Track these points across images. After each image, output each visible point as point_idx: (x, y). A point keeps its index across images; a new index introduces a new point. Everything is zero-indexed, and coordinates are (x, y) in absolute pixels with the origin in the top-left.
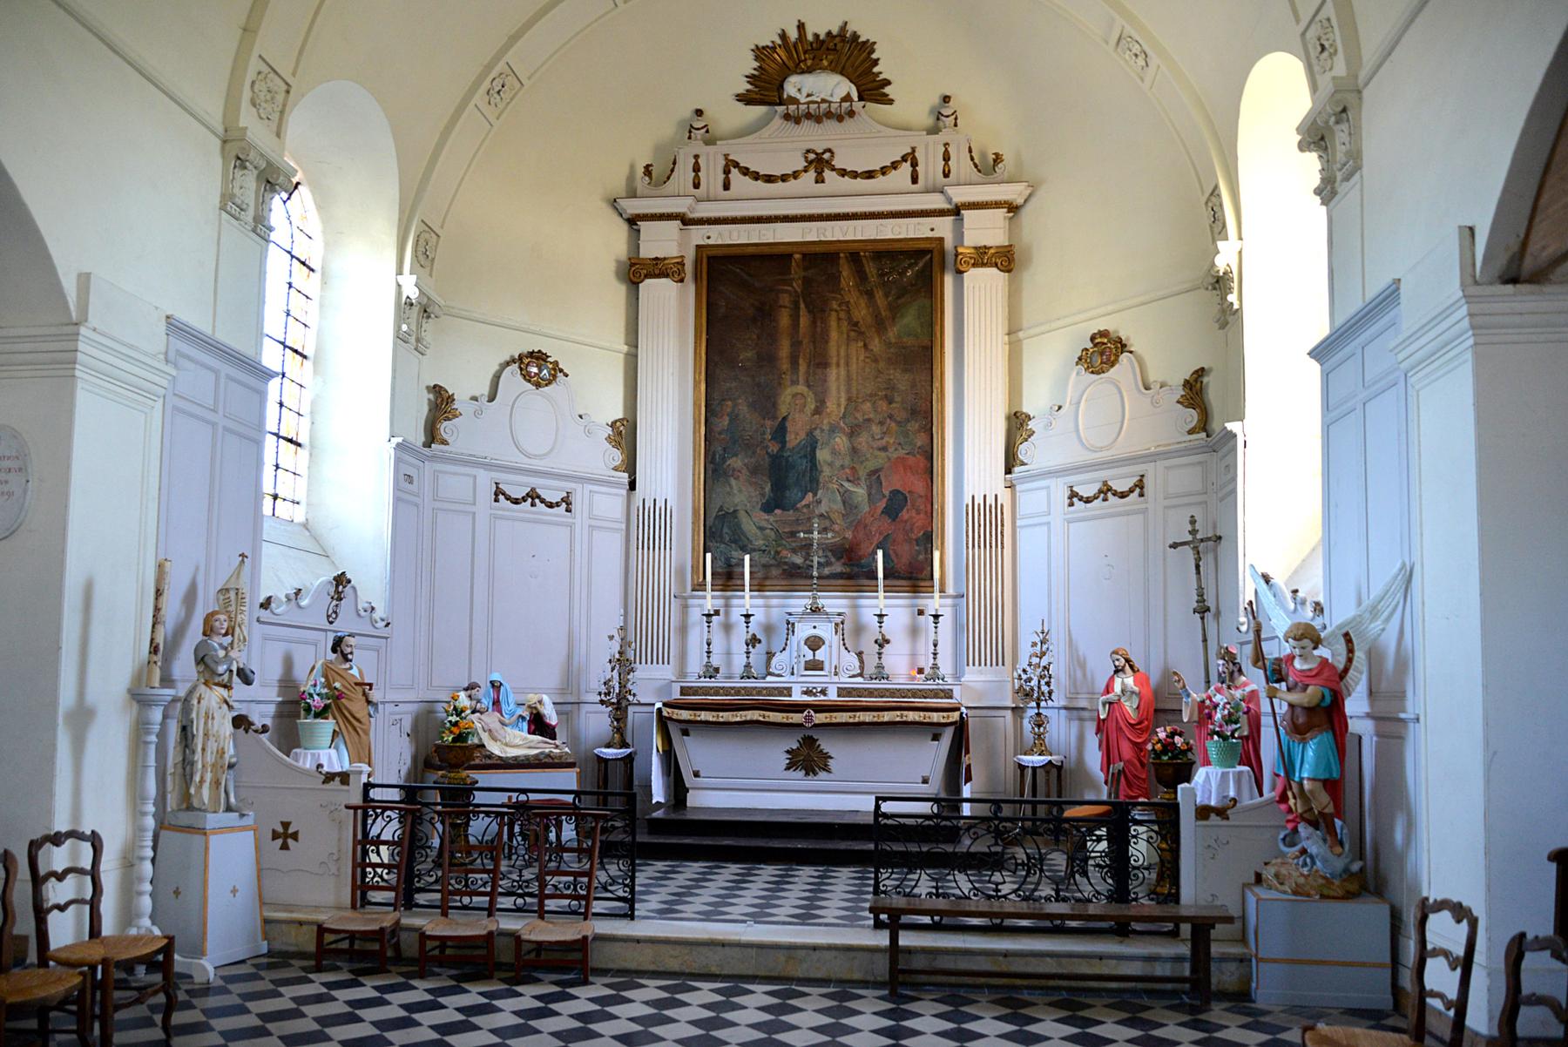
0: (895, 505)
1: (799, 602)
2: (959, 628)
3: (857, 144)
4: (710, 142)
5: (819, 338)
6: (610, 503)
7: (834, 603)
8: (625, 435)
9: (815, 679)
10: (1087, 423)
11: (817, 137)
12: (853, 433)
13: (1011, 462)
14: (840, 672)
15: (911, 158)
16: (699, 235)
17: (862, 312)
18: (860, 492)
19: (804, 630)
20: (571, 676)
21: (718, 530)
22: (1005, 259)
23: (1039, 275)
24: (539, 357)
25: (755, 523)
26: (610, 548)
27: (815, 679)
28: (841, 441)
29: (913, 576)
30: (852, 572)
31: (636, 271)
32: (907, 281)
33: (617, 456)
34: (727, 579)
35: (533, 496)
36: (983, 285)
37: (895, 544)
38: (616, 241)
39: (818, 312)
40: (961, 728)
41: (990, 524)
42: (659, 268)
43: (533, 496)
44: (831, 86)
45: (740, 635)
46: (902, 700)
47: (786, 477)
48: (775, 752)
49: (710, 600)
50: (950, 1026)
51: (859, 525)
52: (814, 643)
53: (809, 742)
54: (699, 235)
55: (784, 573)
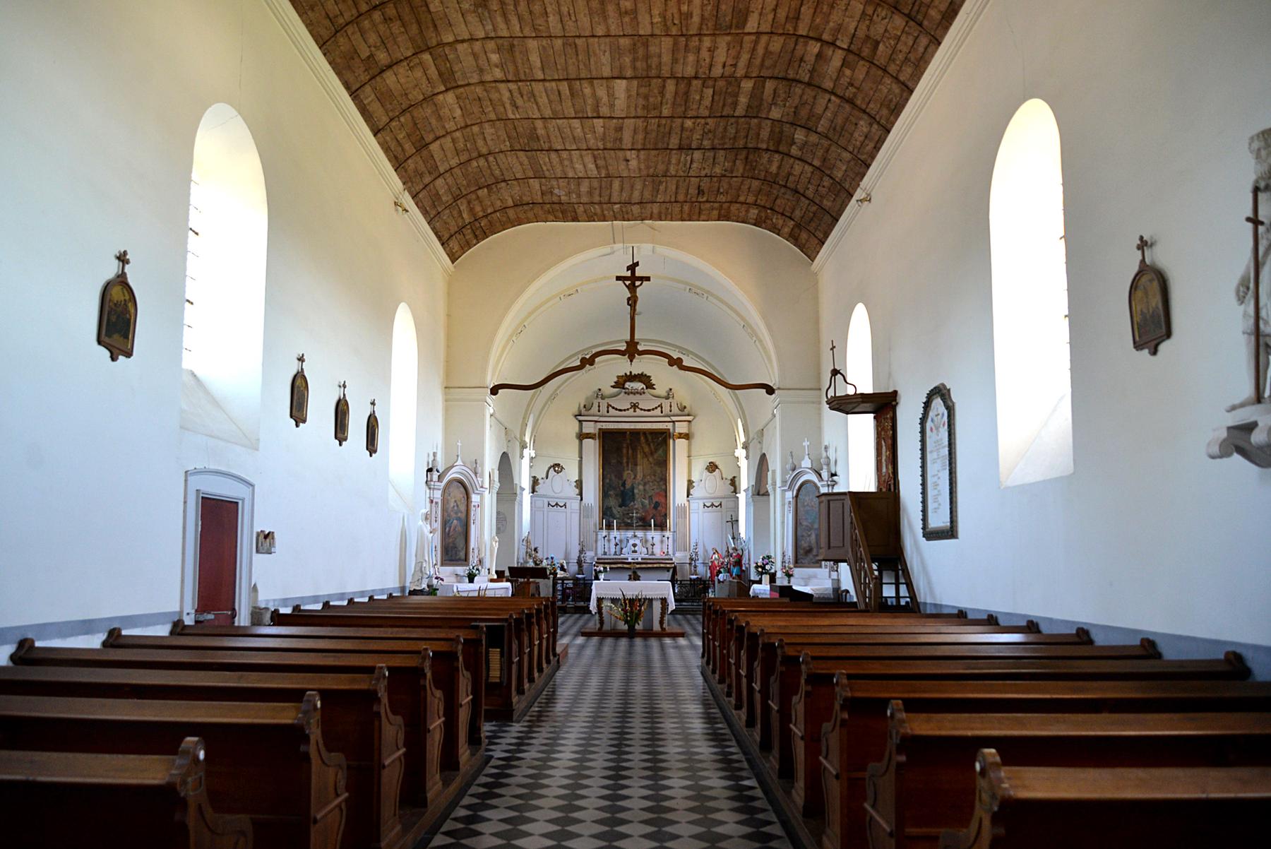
0: (657, 505)
1: (630, 534)
2: (674, 541)
3: (646, 402)
4: (603, 398)
5: (635, 457)
6: (575, 505)
7: (640, 534)
8: (579, 484)
9: (635, 555)
10: (707, 486)
11: (634, 399)
12: (645, 484)
14: (642, 554)
15: (661, 406)
16: (599, 426)
17: (647, 450)
18: (647, 502)
19: (631, 542)
21: (606, 513)
22: (687, 436)
23: (696, 441)
24: (558, 465)
25: (616, 510)
26: (576, 517)
28: (641, 487)
29: (662, 526)
30: (645, 526)
31: (582, 436)
32: (660, 440)
33: (577, 491)
34: (609, 527)
36: (681, 444)
39: (634, 450)
40: (675, 568)
41: (683, 511)
42: (588, 436)
44: (639, 386)
45: (613, 542)
46: (659, 561)
47: (625, 497)
49: (604, 533)
50: (702, 830)
51: (647, 511)
52: (634, 545)
53: (635, 573)
54: (599, 426)
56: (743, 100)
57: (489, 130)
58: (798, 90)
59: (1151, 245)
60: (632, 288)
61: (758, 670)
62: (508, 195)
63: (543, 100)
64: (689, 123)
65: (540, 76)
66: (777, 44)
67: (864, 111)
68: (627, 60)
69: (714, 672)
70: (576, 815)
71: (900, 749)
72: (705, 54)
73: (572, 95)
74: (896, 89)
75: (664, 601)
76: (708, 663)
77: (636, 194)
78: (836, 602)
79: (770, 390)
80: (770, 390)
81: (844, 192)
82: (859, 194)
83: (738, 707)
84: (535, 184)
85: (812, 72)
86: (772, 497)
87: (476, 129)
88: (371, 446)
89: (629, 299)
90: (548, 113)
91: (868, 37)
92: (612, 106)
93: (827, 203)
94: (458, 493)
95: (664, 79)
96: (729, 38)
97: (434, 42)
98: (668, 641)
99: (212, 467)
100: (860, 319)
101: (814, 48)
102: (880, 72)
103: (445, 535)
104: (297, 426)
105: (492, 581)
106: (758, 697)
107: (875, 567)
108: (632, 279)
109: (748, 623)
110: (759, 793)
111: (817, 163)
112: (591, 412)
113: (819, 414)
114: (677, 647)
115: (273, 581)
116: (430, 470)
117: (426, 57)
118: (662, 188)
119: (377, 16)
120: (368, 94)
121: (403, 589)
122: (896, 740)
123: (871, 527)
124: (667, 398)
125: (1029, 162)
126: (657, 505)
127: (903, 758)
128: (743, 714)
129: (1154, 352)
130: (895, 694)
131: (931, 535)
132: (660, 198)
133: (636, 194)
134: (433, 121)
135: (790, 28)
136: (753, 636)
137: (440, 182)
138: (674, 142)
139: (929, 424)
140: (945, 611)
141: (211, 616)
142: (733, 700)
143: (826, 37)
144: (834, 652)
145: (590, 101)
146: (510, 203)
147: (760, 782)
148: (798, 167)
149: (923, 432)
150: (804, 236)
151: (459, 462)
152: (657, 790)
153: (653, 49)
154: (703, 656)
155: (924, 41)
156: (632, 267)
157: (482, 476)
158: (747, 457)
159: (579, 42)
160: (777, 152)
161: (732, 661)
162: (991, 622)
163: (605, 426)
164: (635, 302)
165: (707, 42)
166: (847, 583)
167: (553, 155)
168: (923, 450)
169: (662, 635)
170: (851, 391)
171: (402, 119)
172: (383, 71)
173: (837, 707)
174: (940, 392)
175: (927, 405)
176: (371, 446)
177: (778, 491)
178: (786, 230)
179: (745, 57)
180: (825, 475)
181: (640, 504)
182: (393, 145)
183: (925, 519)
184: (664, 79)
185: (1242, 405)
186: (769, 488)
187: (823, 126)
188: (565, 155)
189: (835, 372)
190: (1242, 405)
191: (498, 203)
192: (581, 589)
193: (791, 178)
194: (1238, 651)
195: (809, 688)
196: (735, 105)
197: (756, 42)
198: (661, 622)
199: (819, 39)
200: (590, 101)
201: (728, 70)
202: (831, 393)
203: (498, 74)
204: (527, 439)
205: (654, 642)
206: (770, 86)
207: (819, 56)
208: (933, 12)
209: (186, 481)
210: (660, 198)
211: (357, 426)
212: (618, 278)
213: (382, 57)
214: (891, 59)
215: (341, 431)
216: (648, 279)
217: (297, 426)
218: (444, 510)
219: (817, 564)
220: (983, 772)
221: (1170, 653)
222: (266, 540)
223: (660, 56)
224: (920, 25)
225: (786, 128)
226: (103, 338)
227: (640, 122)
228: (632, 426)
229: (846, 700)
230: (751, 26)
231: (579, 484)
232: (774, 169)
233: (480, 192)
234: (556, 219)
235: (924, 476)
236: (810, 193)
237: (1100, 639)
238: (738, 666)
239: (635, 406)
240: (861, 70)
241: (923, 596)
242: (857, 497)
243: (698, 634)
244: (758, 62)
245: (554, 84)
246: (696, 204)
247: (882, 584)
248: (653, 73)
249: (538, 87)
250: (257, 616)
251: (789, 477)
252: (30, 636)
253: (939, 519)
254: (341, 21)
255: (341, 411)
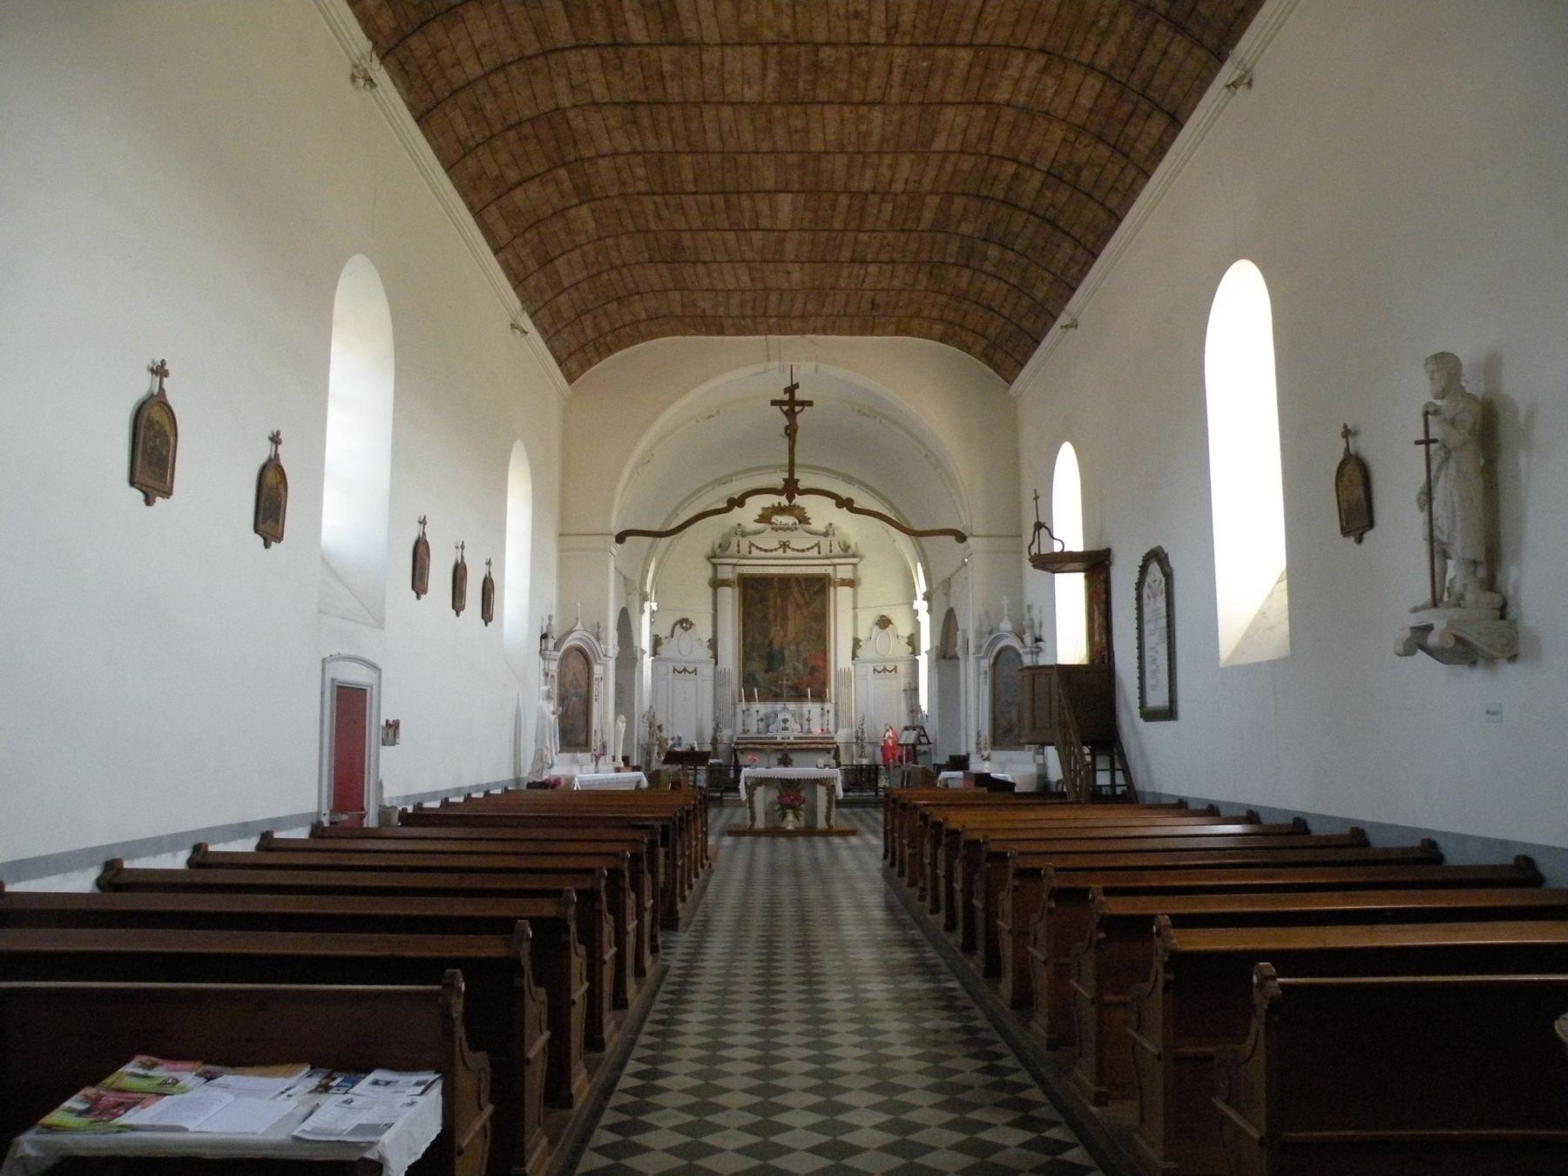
1: (779, 706)
3: (799, 540)
4: (744, 534)
5: (784, 607)
6: (707, 671)
7: (791, 706)
8: (713, 644)
9: (785, 733)
12: (797, 644)
13: (854, 656)
14: (794, 732)
15: (818, 545)
17: (801, 601)
18: (800, 666)
20: (700, 735)
21: (748, 680)
22: (851, 583)
23: (863, 590)
27: (785, 733)
28: (793, 647)
29: (820, 697)
30: (799, 696)
31: (716, 584)
32: (818, 587)
33: (710, 653)
35: (685, 670)
37: (812, 682)
38: (707, 572)
39: (784, 599)
42: (725, 583)
43: (685, 670)
47: (773, 660)
48: (775, 758)
49: (744, 705)
52: (785, 721)
55: (777, 697)
56: (928, 215)
57: (625, 242)
58: (992, 207)
59: (1356, 433)
60: (791, 415)
61: (960, 869)
62: (640, 308)
63: (694, 212)
64: (864, 237)
65: (691, 188)
66: (967, 164)
67: (1068, 234)
68: (795, 175)
69: (901, 874)
70: (724, 1053)
71: (1100, 927)
72: (884, 170)
73: (728, 208)
74: (1103, 215)
75: (831, 790)
76: (892, 865)
77: (798, 306)
78: (1044, 793)
79: (961, 537)
80: (961, 537)
81: (1046, 314)
82: (1063, 319)
83: (934, 911)
84: (676, 296)
85: (1009, 189)
86: (962, 663)
87: (610, 241)
88: (487, 614)
89: (787, 428)
90: (697, 224)
91: (1070, 163)
92: (774, 218)
93: (1027, 324)
94: (577, 664)
95: (837, 194)
96: (912, 156)
97: (572, 157)
98: (837, 840)
99: (346, 652)
100: (1067, 464)
101: (1011, 168)
102: (1083, 197)
103: (563, 718)
104: (267, 546)
105: (618, 770)
106: (959, 898)
107: (1086, 750)
108: (791, 404)
109: (946, 819)
110: (961, 993)
111: (1013, 280)
112: (729, 552)
113: (1020, 578)
114: (851, 848)
115: (405, 776)
116: (544, 637)
117: (562, 172)
118: (829, 300)
119: (512, 135)
120: (492, 214)
121: (517, 781)
122: (1096, 919)
123: (1083, 706)
124: (826, 535)
125: (1241, 323)
126: (813, 670)
127: (1102, 935)
128: (941, 918)
129: (1359, 540)
130: (1096, 885)
131: (1150, 715)
132: (826, 311)
133: (798, 306)
134: (562, 236)
135: (982, 148)
136: (955, 833)
137: (563, 298)
138: (846, 254)
139: (1146, 591)
140: (1165, 801)
141: (345, 817)
142: (928, 904)
143: (1023, 158)
144: (1044, 847)
145: (748, 214)
146: (643, 316)
147: (963, 984)
148: (992, 285)
149: (1139, 598)
150: (999, 356)
151: (579, 626)
152: (767, 1086)
153: (825, 165)
154: (885, 857)
155: (1131, 173)
156: (791, 390)
157: (606, 643)
158: (929, 611)
159: (742, 158)
160: (967, 266)
161: (927, 861)
162: (1212, 812)
163: (746, 570)
164: (795, 432)
165: (888, 159)
166: (1055, 773)
167: (701, 269)
168: (1140, 619)
169: (828, 833)
170: (1057, 548)
171: (527, 235)
172: (510, 189)
173: (1044, 896)
174: (1156, 556)
175: (1143, 570)
176: (487, 614)
177: (972, 658)
178: (979, 348)
179: (931, 174)
180: (1028, 639)
181: (792, 667)
182: (514, 263)
183: (1142, 697)
184: (837, 194)
185: (1423, 608)
186: (959, 651)
187: (1020, 244)
188: (714, 267)
189: (1039, 526)
190: (1423, 608)
191: (628, 318)
192: (724, 781)
193: (985, 295)
194: (1433, 838)
195: (1017, 883)
196: (919, 219)
197: (944, 160)
198: (828, 819)
199: (1015, 160)
200: (748, 214)
201: (911, 186)
202: (1034, 550)
203: (642, 186)
204: (648, 589)
205: (819, 842)
206: (958, 203)
207: (1016, 176)
208: (1139, 146)
209: (323, 669)
210: (826, 311)
211: (474, 592)
212: (774, 403)
213: (513, 175)
214: (1096, 185)
215: (458, 602)
216: (810, 403)
217: (267, 546)
218: (562, 685)
219: (1019, 746)
220: (1158, 933)
221: (1377, 841)
222: (392, 730)
223: (833, 171)
224: (1127, 156)
225: (980, 245)
226: (261, 526)
227: (807, 236)
228: (782, 571)
229: (1053, 890)
230: (939, 144)
231: (713, 644)
232: (963, 284)
233: (608, 306)
234: (698, 333)
235: (1141, 648)
236: (1007, 311)
237: (1316, 829)
238: (934, 866)
239: (785, 546)
240: (1063, 195)
241: (1142, 783)
242: (1068, 671)
243: (874, 832)
244: (945, 178)
245: (707, 197)
246: (868, 319)
247: (1094, 771)
248: (824, 187)
249: (689, 201)
250: (384, 813)
251: (986, 643)
252: (202, 840)
253: (1158, 699)
254: (471, 143)
255: (459, 574)
